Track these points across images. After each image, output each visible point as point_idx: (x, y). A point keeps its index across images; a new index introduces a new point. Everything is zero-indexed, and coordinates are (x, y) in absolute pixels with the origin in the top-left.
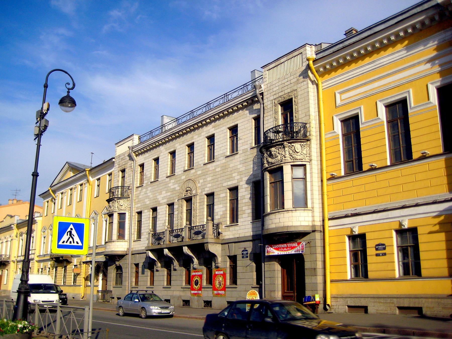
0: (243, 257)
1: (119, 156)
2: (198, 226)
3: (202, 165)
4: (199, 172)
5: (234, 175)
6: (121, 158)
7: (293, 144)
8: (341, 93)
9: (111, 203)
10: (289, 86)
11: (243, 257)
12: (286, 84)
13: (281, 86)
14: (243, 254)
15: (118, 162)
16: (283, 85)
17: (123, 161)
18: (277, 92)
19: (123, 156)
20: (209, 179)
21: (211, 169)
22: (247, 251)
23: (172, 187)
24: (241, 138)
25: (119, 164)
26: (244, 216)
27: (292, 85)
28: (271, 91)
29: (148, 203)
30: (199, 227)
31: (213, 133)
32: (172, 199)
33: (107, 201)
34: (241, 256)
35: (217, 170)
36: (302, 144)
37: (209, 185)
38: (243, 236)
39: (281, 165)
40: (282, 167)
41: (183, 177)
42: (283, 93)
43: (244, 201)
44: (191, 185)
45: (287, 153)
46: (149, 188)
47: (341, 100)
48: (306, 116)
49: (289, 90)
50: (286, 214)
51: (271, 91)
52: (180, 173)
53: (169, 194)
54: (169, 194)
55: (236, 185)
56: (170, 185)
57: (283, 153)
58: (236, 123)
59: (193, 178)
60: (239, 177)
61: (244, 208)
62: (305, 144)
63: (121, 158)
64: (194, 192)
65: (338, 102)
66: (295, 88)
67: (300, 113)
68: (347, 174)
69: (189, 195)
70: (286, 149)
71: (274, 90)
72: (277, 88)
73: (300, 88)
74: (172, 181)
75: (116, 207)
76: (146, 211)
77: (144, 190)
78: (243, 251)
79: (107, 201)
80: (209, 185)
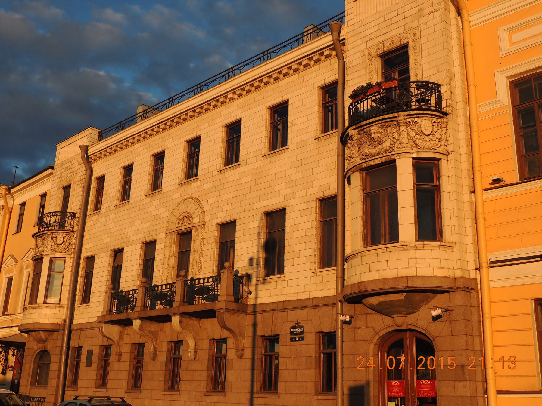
0: (293, 340)
1: (62, 164)
2: (204, 279)
3: (216, 173)
4: (207, 186)
5: (277, 188)
6: (64, 166)
7: (416, 119)
8: (508, 30)
9: (39, 239)
10: (401, 23)
11: (293, 340)
12: (394, 20)
13: (383, 25)
14: (292, 333)
15: (59, 173)
16: (389, 22)
17: (69, 171)
18: (375, 35)
19: (69, 164)
20: (226, 197)
21: (231, 179)
22: (301, 327)
23: (156, 213)
24: (294, 122)
25: (61, 177)
26: (296, 261)
27: (408, 20)
28: (363, 35)
29: (108, 240)
30: (206, 281)
31: (238, 117)
32: (152, 233)
33: (33, 236)
34: (289, 336)
35: (244, 180)
36: (434, 120)
37: (226, 208)
38: (295, 298)
39: (393, 157)
40: (394, 161)
41: (177, 196)
42: (388, 36)
43: (297, 234)
44: (191, 207)
45: (404, 135)
46: (112, 216)
47: (512, 43)
48: (438, 72)
49: (401, 30)
50: (403, 254)
51: (363, 35)
52: (172, 188)
53: (148, 224)
54: (148, 224)
55: (281, 206)
56: (150, 209)
57: (396, 135)
58: (284, 98)
59: (195, 195)
60: (287, 191)
61: (297, 247)
62: (439, 120)
63: (64, 166)
64: (196, 220)
65: (505, 47)
66: (415, 24)
67: (425, 67)
68: (523, 179)
69: (185, 226)
70: (403, 128)
71: (368, 32)
72: (376, 28)
73: (425, 23)
74: (156, 202)
75: (49, 246)
76: (102, 255)
77: (102, 220)
78: (293, 327)
79: (33, 236)
80: (226, 208)
